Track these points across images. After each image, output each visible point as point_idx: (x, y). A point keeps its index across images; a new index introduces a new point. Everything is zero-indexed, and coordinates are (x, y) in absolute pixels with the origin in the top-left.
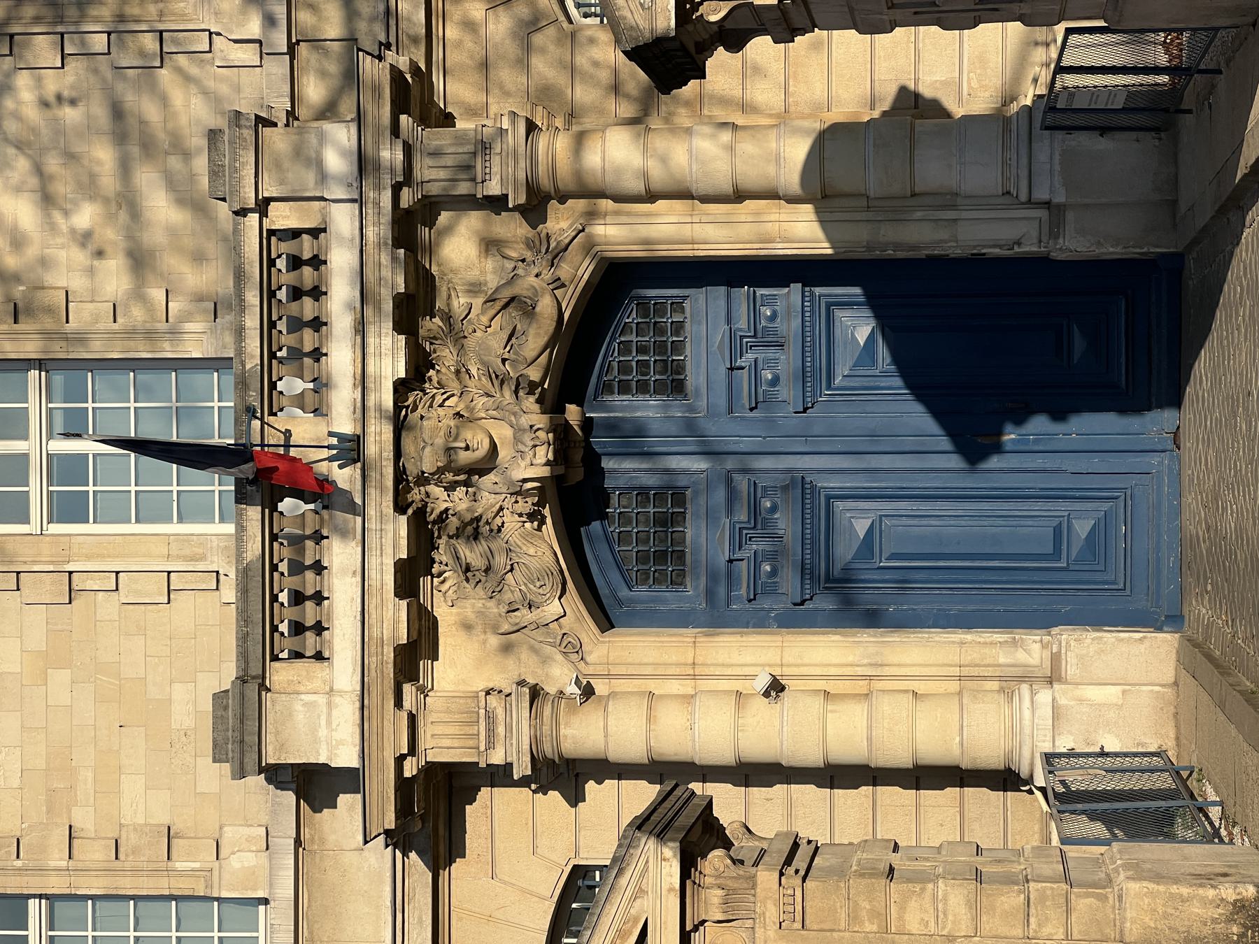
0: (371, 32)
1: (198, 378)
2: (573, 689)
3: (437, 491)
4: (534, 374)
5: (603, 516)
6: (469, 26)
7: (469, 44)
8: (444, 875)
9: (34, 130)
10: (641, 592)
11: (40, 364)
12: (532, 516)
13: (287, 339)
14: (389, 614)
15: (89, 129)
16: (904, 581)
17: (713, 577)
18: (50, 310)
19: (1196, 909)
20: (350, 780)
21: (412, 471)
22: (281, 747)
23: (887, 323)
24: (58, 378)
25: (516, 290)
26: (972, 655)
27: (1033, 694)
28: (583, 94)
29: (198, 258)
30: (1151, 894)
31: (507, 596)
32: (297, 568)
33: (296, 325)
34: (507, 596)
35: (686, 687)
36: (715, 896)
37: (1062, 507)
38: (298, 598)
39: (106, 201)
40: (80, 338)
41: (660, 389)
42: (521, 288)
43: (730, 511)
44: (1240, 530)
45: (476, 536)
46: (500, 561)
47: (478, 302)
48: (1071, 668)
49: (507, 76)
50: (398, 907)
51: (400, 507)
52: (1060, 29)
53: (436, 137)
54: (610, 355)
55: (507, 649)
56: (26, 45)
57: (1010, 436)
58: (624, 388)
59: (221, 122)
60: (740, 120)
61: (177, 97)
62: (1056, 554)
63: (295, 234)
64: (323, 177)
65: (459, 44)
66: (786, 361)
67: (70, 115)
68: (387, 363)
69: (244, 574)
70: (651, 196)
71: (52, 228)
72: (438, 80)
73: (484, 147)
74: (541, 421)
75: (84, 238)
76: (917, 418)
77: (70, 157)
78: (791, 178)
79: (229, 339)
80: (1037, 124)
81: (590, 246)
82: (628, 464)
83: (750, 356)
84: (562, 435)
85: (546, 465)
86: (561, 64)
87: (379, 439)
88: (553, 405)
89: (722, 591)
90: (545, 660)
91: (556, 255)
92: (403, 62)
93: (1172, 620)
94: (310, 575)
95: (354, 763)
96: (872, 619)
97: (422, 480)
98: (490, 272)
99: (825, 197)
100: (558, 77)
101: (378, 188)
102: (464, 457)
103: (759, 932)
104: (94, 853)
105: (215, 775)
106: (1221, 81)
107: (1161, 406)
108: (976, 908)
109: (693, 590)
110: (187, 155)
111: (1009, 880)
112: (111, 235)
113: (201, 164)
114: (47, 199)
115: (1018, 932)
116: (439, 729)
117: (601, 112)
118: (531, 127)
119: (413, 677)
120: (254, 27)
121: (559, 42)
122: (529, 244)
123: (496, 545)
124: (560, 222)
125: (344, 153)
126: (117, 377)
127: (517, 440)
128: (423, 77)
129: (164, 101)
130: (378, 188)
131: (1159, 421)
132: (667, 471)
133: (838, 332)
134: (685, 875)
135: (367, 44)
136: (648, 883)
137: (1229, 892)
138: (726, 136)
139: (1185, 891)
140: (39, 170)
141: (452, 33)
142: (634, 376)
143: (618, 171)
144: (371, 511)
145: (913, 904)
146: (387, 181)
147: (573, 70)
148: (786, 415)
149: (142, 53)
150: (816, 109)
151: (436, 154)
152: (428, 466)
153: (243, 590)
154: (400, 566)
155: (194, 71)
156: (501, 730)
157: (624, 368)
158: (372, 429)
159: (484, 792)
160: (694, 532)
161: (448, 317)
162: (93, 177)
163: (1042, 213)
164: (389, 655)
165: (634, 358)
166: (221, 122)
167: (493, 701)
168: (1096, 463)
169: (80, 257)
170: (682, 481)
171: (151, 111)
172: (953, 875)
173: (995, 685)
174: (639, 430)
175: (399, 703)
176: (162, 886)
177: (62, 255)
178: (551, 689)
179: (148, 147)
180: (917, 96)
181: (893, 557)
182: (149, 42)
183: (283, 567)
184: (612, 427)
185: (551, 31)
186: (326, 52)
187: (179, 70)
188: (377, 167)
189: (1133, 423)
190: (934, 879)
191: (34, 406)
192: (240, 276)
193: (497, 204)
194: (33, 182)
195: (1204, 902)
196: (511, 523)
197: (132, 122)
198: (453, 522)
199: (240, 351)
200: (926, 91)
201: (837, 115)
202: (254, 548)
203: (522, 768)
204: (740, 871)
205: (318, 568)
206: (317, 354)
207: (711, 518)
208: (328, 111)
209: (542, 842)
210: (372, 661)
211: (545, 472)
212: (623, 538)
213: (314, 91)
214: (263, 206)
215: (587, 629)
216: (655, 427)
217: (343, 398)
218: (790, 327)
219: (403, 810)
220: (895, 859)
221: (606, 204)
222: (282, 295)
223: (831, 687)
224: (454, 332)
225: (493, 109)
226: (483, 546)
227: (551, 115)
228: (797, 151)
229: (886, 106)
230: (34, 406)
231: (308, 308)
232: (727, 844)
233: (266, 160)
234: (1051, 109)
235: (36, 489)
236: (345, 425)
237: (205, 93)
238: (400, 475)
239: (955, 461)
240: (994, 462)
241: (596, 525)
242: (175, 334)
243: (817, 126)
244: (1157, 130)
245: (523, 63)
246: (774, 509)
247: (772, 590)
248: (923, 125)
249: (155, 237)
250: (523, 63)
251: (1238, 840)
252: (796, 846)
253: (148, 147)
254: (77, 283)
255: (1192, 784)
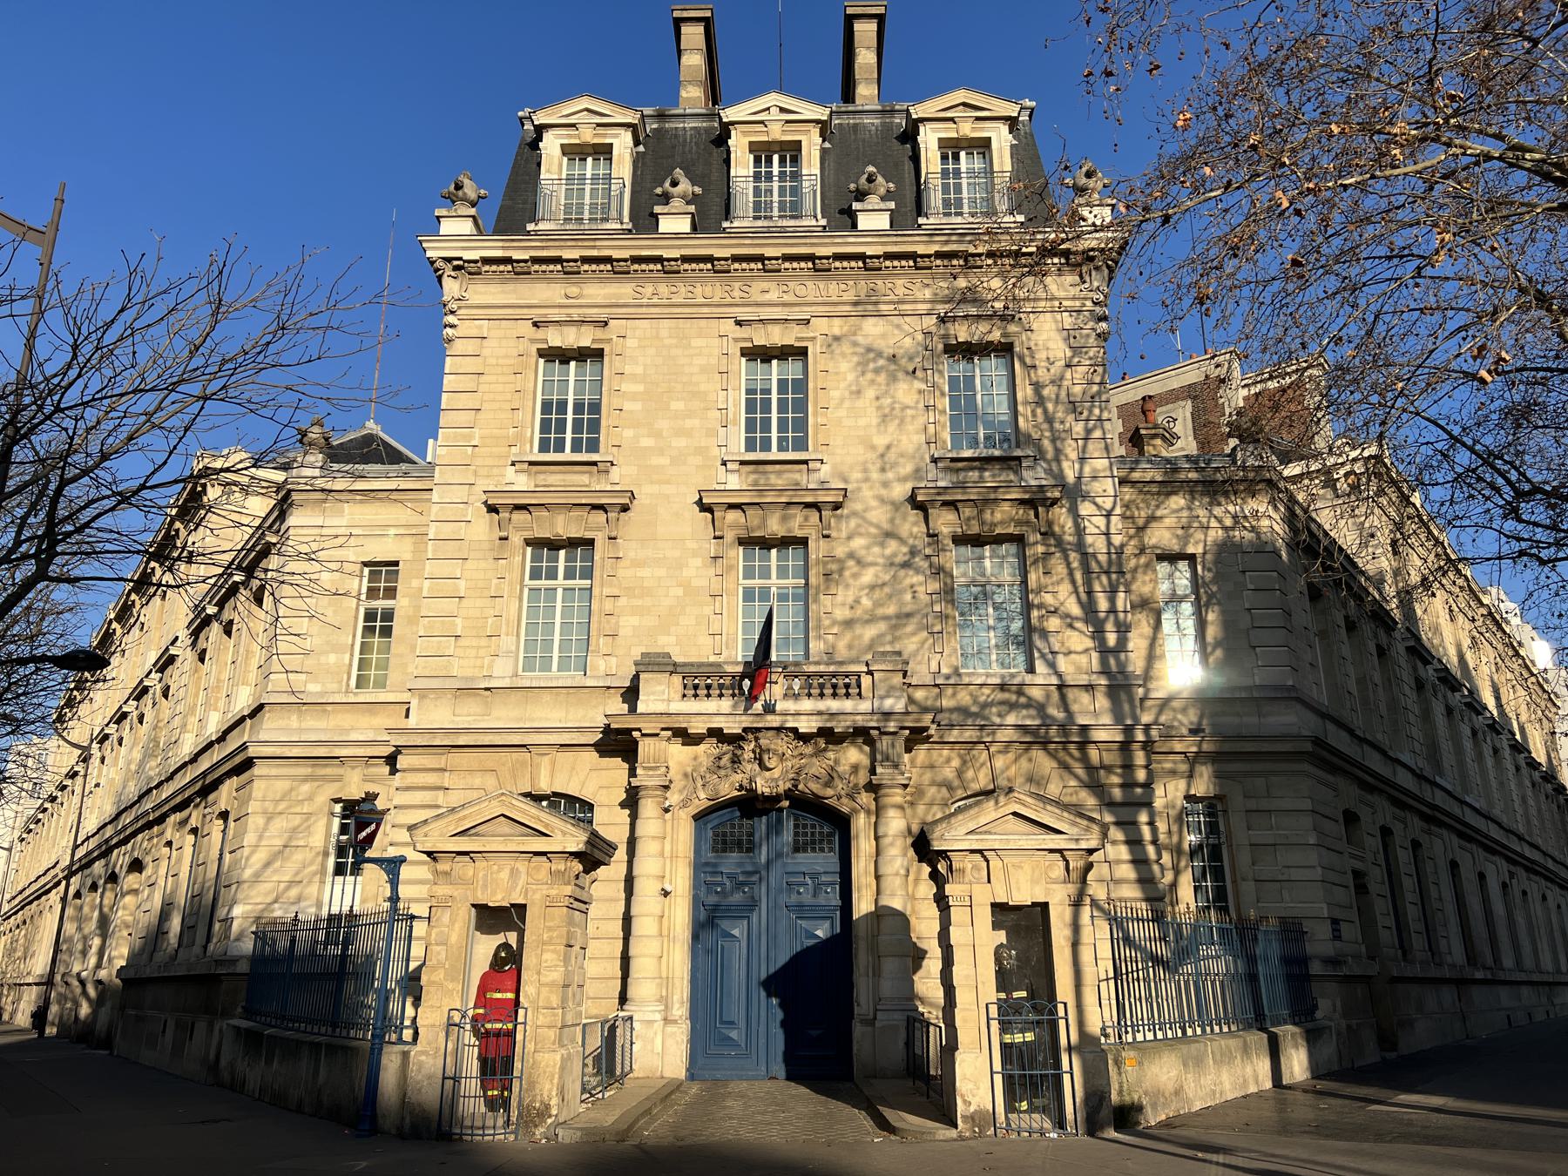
0: (944, 718)
1: (802, 647)
2: (667, 804)
3: (752, 745)
4: (801, 787)
5: (742, 817)
6: (948, 760)
7: (941, 760)
8: (592, 749)
9: (900, 583)
10: (710, 833)
11: (807, 584)
12: (741, 786)
13: (815, 683)
14: (701, 725)
15: (902, 604)
16: (708, 952)
17: (715, 865)
18: (828, 588)
19: (547, 1086)
20: (633, 709)
21: (760, 735)
22: (647, 680)
23: (825, 943)
24: (801, 591)
25: (836, 779)
26: (677, 983)
27: (660, 1011)
28: (921, 809)
29: (850, 647)
30: (555, 1065)
31: (708, 776)
32: (721, 687)
33: (821, 686)
34: (708, 776)
35: (667, 854)
36: (562, 867)
37: (742, 1024)
38: (708, 687)
39: (873, 610)
40: (816, 601)
41: (796, 842)
42: (837, 781)
43: (743, 873)
44: (725, 1108)
45: (733, 762)
46: (722, 772)
47: (831, 763)
48: (670, 1029)
49: (927, 777)
50: (579, 729)
51: (745, 730)
52: (943, 1026)
53: (900, 744)
54: (810, 820)
55: (686, 775)
56: (935, 579)
57: (774, 1001)
58: (796, 826)
59: (905, 656)
60: (911, 878)
61: (916, 639)
62: (722, 1022)
63: (859, 686)
64: (882, 698)
65: (941, 755)
66: (807, 899)
67: (908, 597)
68: (805, 724)
69: (719, 665)
70: (877, 838)
71: (862, 589)
72: (926, 746)
73: (896, 766)
74: (781, 790)
75: (857, 601)
76: (783, 958)
77: (890, 597)
78: (885, 901)
79: (816, 659)
80: (910, 1013)
81: (855, 811)
82: (764, 827)
83: (810, 882)
84: (776, 799)
85: (384, 812)
86: (934, 799)
87: (772, 720)
88: (788, 794)
89: (709, 869)
90: (680, 792)
91: (851, 797)
92: (932, 732)
93: (692, 1075)
94: (718, 692)
95: (639, 710)
96: (695, 937)
97: (757, 739)
98: (843, 768)
99: (878, 916)
100: (927, 799)
101: (878, 721)
102: (766, 757)
103: (545, 887)
104: (608, 605)
105: (636, 653)
106: (924, 1099)
107: (787, 1071)
108: (552, 984)
109: (710, 856)
110: (891, 643)
111: (564, 1000)
112: (859, 612)
113: (888, 648)
114: (872, 587)
115: (541, 1004)
116: (652, 746)
117: (913, 816)
118: (905, 786)
119: (675, 735)
120: (945, 670)
121: (943, 799)
122: (856, 785)
123: (729, 771)
124: (865, 798)
125: (892, 706)
126: (802, 614)
127: (773, 780)
128: (927, 740)
129: (914, 634)
130: (878, 721)
131: (779, 1069)
132: (761, 845)
133: (821, 922)
134: (571, 854)
135: (939, 717)
136: (568, 837)
137: (554, 1102)
138: (903, 872)
139: (556, 1081)
140: (884, 584)
141: (945, 752)
142: (801, 830)
143: (887, 824)
144: (744, 718)
145: (554, 956)
146: (882, 724)
147: (931, 804)
148: (784, 899)
149: (933, 625)
150: (913, 911)
151: (893, 746)
152: (762, 742)
153: (711, 665)
154: (721, 730)
155: (926, 646)
156: (651, 773)
157: (805, 826)
158: (777, 718)
159: (627, 766)
160: (734, 856)
161: (825, 750)
162: (882, 605)
163: (871, 1016)
164: (683, 725)
165: (809, 830)
166: (905, 656)
167: (663, 770)
168: (762, 1041)
169: (850, 600)
170: (756, 851)
171: (909, 629)
172: (567, 974)
173: (664, 994)
174: (778, 833)
175: (663, 729)
176: (593, 633)
177: (850, 593)
178: (668, 795)
179: (895, 627)
180: (923, 958)
181: (722, 947)
182: (937, 628)
183: (722, 681)
184: (779, 821)
185: (947, 795)
186: (936, 699)
187: (926, 639)
188: (887, 720)
189: (780, 1058)
190: (566, 966)
191: (790, 581)
192: (841, 663)
193: (873, 771)
194: (880, 582)
195: (550, 1090)
196: (738, 777)
197: (904, 621)
198: (739, 752)
199: (810, 663)
200: (925, 963)
201: (913, 921)
202: (729, 669)
203: (635, 782)
204: (572, 878)
205: (721, 695)
206: (809, 695)
207: (740, 864)
208: (911, 700)
209: (604, 791)
210: (681, 718)
211: (759, 792)
212: (733, 826)
213: (919, 695)
214: (870, 673)
215: (693, 810)
216: (779, 840)
217: (790, 705)
218: (821, 900)
219: (619, 731)
220: (577, 948)
221: (873, 819)
222: (834, 681)
223: (665, 919)
224: (819, 753)
225: (914, 770)
226: (729, 765)
227: (912, 795)
228: (897, 904)
229: (919, 945)
230: (790, 581)
231: (828, 691)
232: (586, 871)
233: (889, 674)
234: (915, 1020)
235: (757, 582)
236: (778, 707)
237: (918, 650)
238: (759, 730)
239: (764, 976)
240: (763, 994)
241: (738, 814)
242: (819, 637)
243: (908, 913)
244: (908, 1069)
245: (933, 783)
246: (744, 892)
247: (709, 892)
248: (910, 961)
249: (858, 630)
250: (933, 783)
251: (584, 1105)
252: (585, 903)
253: (895, 627)
254: (839, 599)
255: (617, 1084)
